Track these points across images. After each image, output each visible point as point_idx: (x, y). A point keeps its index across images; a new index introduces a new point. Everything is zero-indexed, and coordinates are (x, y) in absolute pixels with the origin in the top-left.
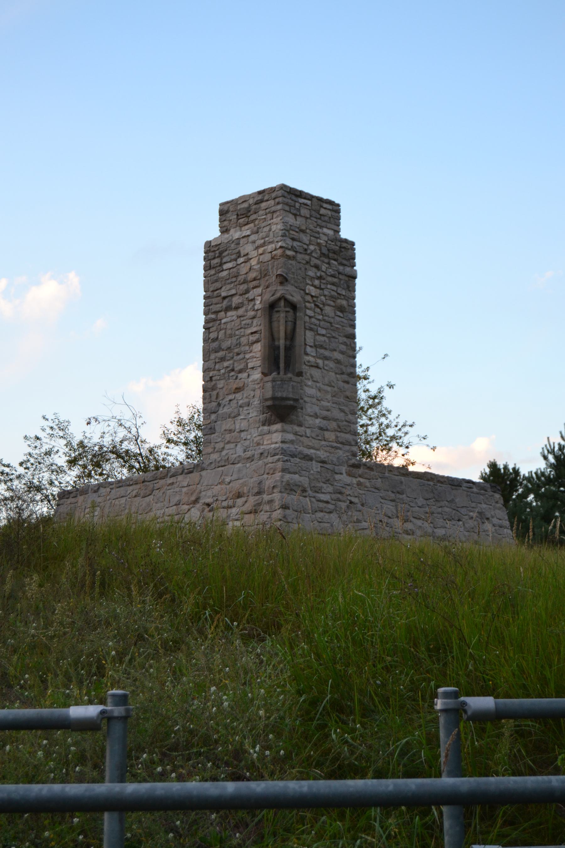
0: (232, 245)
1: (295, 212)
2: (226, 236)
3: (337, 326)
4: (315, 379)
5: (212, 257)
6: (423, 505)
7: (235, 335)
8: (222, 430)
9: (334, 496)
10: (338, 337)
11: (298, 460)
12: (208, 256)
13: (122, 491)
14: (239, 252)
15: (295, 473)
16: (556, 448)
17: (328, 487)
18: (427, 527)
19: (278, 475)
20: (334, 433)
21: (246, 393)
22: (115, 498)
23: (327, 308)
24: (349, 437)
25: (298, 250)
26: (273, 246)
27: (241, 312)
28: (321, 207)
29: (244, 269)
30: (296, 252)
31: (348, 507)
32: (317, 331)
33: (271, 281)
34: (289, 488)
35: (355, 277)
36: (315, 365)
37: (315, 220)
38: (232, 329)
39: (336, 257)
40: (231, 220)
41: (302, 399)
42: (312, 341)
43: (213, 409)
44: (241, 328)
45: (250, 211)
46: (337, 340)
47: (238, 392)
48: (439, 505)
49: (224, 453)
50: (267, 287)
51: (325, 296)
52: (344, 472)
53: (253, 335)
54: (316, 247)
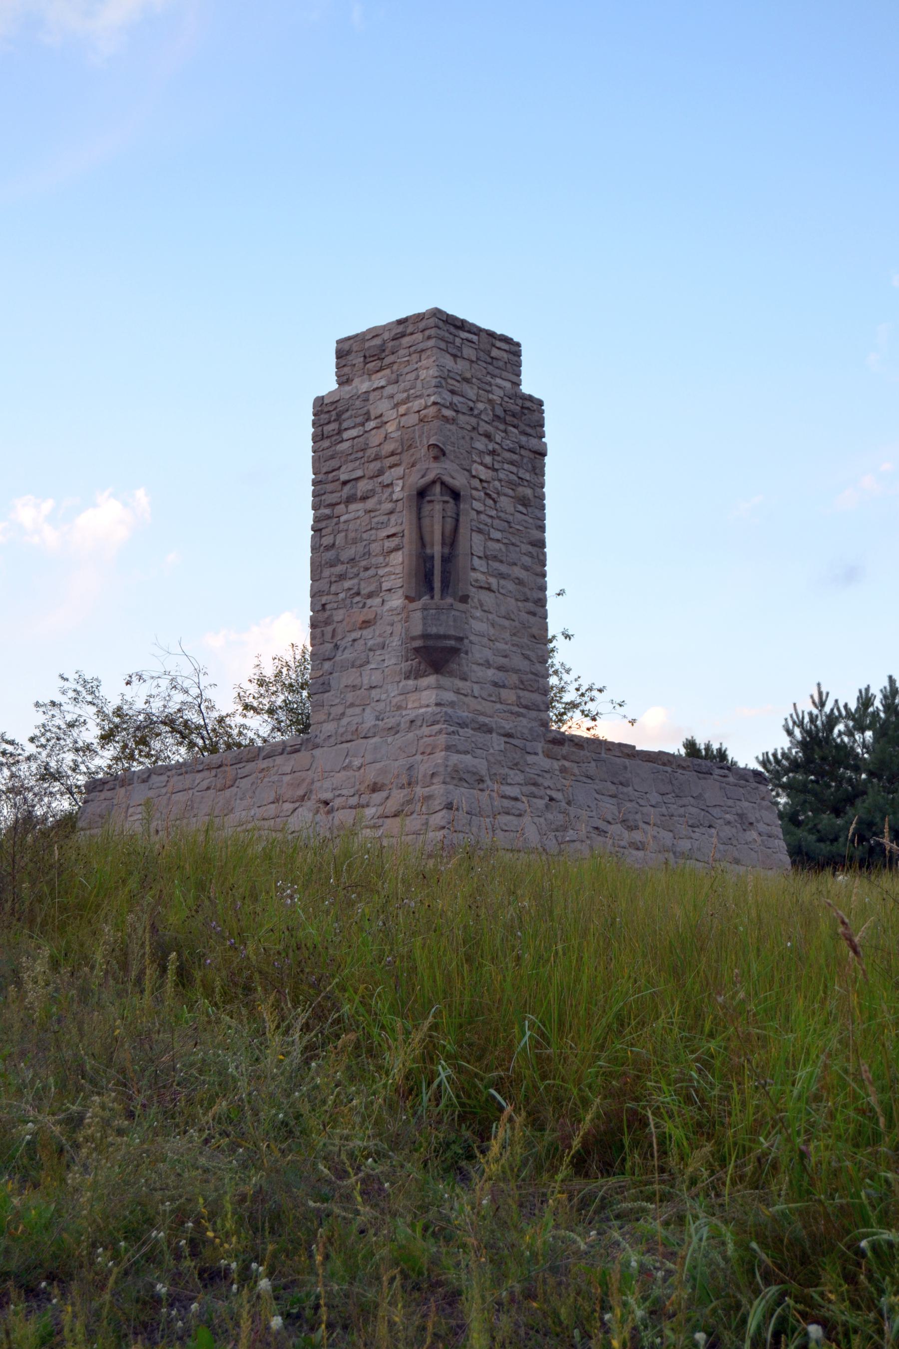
0: (357, 402)
1: (454, 351)
2: (347, 388)
3: (518, 527)
4: (486, 608)
5: (326, 422)
6: (658, 803)
7: (362, 540)
8: (342, 686)
9: (525, 789)
10: (518, 543)
11: (471, 732)
12: (319, 420)
13: (188, 780)
14: (368, 413)
15: (466, 752)
16: (807, 719)
17: (516, 775)
18: (667, 837)
19: (439, 756)
20: (514, 691)
21: (378, 628)
22: (507, 847)
23: (502, 498)
24: (536, 697)
25: (460, 409)
26: (423, 401)
27: (370, 504)
28: (493, 345)
29: (375, 438)
30: (457, 411)
31: (547, 806)
32: (489, 535)
33: (419, 456)
34: (458, 777)
35: (543, 454)
36: (487, 586)
37: (485, 365)
38: (356, 530)
39: (516, 422)
40: (354, 365)
41: (467, 638)
42: (482, 549)
43: (327, 653)
44: (371, 529)
45: (384, 351)
46: (518, 549)
47: (366, 628)
48: (681, 802)
49: (344, 721)
50: (413, 466)
51: (500, 480)
52: (540, 751)
53: (390, 539)
54: (487, 405)
